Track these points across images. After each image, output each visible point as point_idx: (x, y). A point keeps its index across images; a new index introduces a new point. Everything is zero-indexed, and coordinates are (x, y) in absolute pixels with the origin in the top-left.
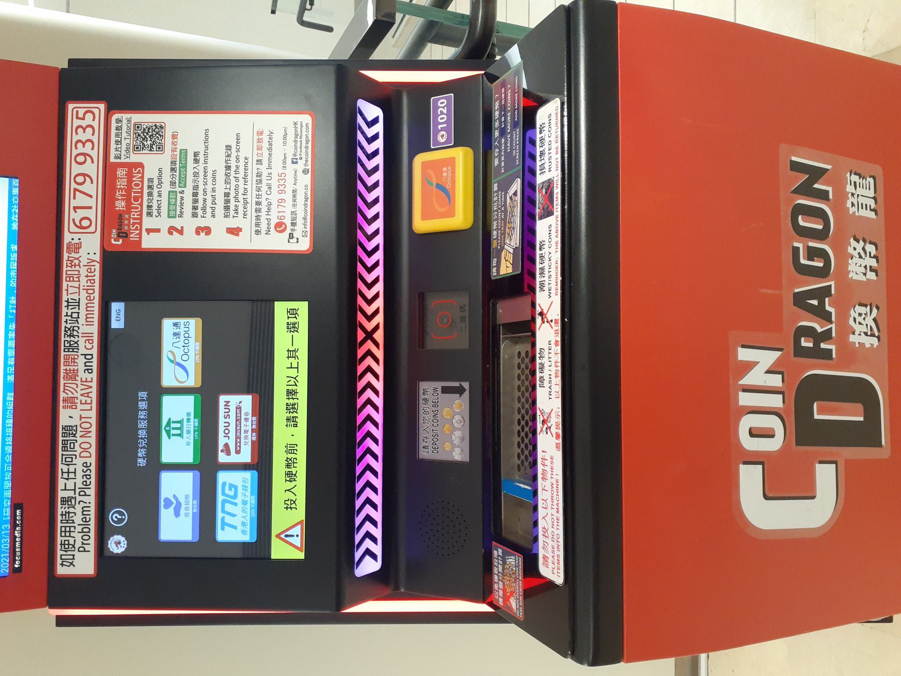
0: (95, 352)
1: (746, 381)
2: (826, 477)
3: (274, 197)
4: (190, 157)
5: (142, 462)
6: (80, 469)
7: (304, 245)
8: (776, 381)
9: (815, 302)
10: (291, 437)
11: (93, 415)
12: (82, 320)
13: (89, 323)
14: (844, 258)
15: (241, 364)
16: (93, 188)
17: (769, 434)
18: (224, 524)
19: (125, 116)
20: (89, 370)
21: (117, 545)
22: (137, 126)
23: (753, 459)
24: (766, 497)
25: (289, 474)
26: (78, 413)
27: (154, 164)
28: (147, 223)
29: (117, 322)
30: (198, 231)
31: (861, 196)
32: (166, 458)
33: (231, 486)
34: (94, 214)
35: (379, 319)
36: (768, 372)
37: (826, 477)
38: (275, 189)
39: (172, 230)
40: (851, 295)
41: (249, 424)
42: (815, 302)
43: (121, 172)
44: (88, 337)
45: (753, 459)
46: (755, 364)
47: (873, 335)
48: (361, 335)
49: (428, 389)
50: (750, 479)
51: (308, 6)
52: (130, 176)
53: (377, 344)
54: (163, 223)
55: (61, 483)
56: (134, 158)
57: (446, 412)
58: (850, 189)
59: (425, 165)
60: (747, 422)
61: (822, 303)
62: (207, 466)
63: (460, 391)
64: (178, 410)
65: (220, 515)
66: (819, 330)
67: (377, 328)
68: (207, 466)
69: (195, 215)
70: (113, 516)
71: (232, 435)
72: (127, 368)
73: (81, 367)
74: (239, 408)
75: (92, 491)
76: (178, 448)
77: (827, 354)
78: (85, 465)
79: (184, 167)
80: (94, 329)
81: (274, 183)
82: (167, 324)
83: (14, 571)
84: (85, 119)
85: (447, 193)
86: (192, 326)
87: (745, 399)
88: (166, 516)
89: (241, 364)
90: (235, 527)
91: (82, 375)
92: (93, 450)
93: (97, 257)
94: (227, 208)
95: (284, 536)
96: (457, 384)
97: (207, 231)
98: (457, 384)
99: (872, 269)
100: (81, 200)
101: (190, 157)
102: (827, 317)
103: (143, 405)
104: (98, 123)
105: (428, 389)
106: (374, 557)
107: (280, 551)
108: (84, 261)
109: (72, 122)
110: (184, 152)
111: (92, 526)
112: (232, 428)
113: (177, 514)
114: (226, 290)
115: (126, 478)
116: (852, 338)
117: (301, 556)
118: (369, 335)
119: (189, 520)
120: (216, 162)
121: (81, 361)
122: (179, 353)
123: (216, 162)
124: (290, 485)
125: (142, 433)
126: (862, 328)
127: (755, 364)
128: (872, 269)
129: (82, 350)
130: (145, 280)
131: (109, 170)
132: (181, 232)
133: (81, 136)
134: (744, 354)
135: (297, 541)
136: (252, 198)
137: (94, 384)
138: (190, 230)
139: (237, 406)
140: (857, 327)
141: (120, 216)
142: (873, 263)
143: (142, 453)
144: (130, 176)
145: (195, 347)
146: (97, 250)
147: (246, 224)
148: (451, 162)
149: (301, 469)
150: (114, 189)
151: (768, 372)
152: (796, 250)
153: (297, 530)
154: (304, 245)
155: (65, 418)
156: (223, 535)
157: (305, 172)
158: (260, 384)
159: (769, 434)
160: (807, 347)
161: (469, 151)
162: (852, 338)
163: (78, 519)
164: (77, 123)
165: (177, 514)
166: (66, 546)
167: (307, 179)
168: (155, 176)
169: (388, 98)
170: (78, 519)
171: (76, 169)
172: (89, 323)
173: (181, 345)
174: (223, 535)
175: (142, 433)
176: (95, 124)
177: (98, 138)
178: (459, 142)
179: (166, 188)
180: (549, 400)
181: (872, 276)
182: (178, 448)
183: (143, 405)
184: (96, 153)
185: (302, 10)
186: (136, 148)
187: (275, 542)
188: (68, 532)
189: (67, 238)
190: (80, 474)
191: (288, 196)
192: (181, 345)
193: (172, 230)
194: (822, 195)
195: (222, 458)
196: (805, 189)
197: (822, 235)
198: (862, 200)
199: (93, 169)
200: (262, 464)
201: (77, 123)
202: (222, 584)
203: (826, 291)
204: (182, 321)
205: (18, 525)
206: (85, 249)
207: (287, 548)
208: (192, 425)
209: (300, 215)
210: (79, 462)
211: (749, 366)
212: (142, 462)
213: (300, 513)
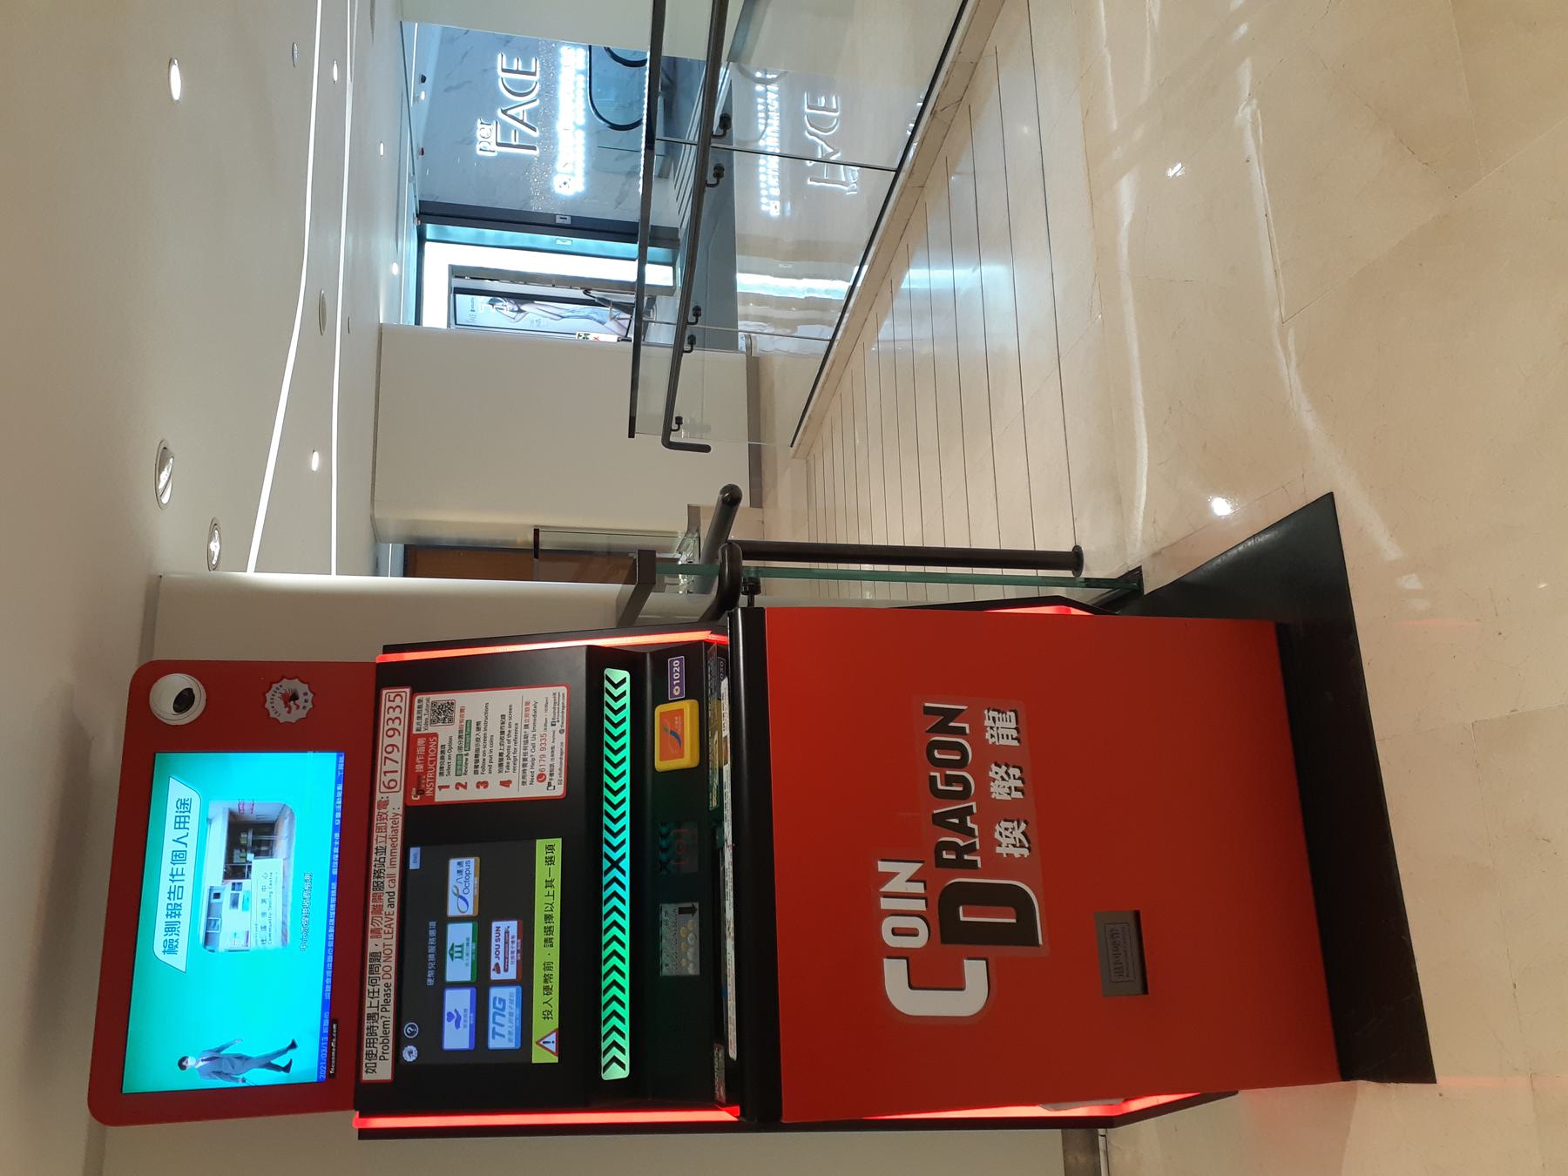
0: (396, 890)
1: (888, 887)
2: (975, 972)
3: (537, 754)
4: (474, 726)
5: (430, 982)
6: (382, 988)
7: (559, 791)
8: (918, 888)
9: (956, 821)
10: (548, 955)
11: (393, 943)
12: (387, 864)
13: (393, 866)
14: (985, 782)
15: (506, 895)
16: (399, 756)
17: (913, 933)
18: (495, 1033)
19: (424, 697)
20: (391, 905)
21: (410, 1054)
22: (434, 704)
23: (897, 954)
25: (546, 988)
26: (382, 942)
27: (446, 733)
28: (440, 781)
29: (414, 865)
30: (479, 785)
31: (1002, 728)
33: (502, 1001)
34: (399, 777)
35: (626, 849)
36: (909, 881)
37: (975, 972)
38: (538, 747)
39: (458, 785)
42: (956, 821)
43: (421, 742)
44: (391, 876)
45: (897, 954)
46: (894, 875)
47: (1022, 846)
48: (606, 864)
50: (895, 974)
51: (674, 426)
52: (427, 744)
53: (623, 872)
54: (451, 780)
55: (368, 1002)
56: (431, 730)
58: (988, 723)
60: (888, 924)
61: (963, 821)
62: (481, 984)
63: (691, 911)
64: (460, 935)
65: (491, 1025)
66: (962, 844)
67: (623, 856)
68: (481, 984)
69: (476, 772)
70: (407, 1029)
71: (502, 956)
72: (422, 902)
73: (386, 903)
74: (507, 933)
75: (391, 1008)
76: (459, 969)
78: (387, 985)
79: (469, 734)
80: (396, 871)
81: (537, 742)
83: (328, 1074)
84: (395, 701)
85: (679, 738)
86: (471, 864)
87: (886, 904)
88: (449, 1027)
89: (506, 895)
90: (503, 1037)
91: (386, 909)
92: (393, 973)
93: (400, 812)
94: (501, 765)
95: (542, 1043)
96: (689, 905)
97: (485, 784)
98: (689, 905)
99: (1017, 789)
100: (389, 766)
101: (474, 726)
102: (971, 832)
103: (432, 933)
104: (405, 704)
105: (668, 912)
106: (622, 1065)
108: (390, 815)
109: (385, 704)
110: (469, 722)
111: (391, 1036)
112: (502, 950)
113: (457, 1025)
114: (498, 830)
115: (419, 999)
116: (998, 850)
117: (555, 1059)
118: (615, 864)
119: (467, 1030)
120: (494, 729)
121: (386, 897)
123: (494, 729)
124: (547, 998)
125: (431, 957)
126: (1010, 840)
127: (894, 875)
128: (1017, 789)
129: (387, 889)
130: (439, 828)
131: (412, 740)
132: (465, 787)
133: (392, 715)
134: (883, 867)
135: (553, 1047)
136: (520, 757)
137: (395, 917)
138: (472, 785)
140: (1004, 841)
141: (419, 776)
142: (1019, 784)
143: (430, 974)
144: (427, 744)
145: (473, 881)
146: (400, 804)
147: (514, 777)
148: (681, 712)
149: (555, 983)
150: (415, 755)
151: (909, 881)
153: (553, 1037)
154: (559, 791)
155: (373, 945)
156: (494, 1043)
157: (561, 732)
159: (913, 933)
160: (936, 862)
161: (695, 702)
162: (998, 850)
163: (380, 1032)
164: (389, 704)
165: (457, 1025)
166: (370, 1055)
167: (562, 738)
168: (446, 743)
170: (380, 1032)
171: (387, 741)
172: (393, 866)
173: (463, 879)
174: (494, 1043)
175: (431, 957)
176: (400, 728)
177: (404, 716)
178: (688, 696)
179: (455, 751)
180: (729, 914)
181: (1019, 795)
182: (459, 969)
183: (432, 933)
184: (402, 728)
185: (667, 431)
186: (433, 722)
187: (535, 1048)
188: (372, 1043)
189: (378, 797)
190: (382, 993)
191: (548, 752)
192: (463, 879)
193: (458, 785)
194: (960, 732)
195: (494, 976)
196: (942, 728)
197: (960, 764)
198: (1005, 732)
199: (400, 740)
200: (524, 980)
201: (389, 704)
202: (492, 1082)
203: (969, 810)
204: (464, 860)
205: (586, 292)
206: (391, 803)
207: (544, 1054)
208: (470, 948)
209: (557, 767)
210: (382, 983)
211: (890, 876)
212: (430, 982)
213: (554, 1023)
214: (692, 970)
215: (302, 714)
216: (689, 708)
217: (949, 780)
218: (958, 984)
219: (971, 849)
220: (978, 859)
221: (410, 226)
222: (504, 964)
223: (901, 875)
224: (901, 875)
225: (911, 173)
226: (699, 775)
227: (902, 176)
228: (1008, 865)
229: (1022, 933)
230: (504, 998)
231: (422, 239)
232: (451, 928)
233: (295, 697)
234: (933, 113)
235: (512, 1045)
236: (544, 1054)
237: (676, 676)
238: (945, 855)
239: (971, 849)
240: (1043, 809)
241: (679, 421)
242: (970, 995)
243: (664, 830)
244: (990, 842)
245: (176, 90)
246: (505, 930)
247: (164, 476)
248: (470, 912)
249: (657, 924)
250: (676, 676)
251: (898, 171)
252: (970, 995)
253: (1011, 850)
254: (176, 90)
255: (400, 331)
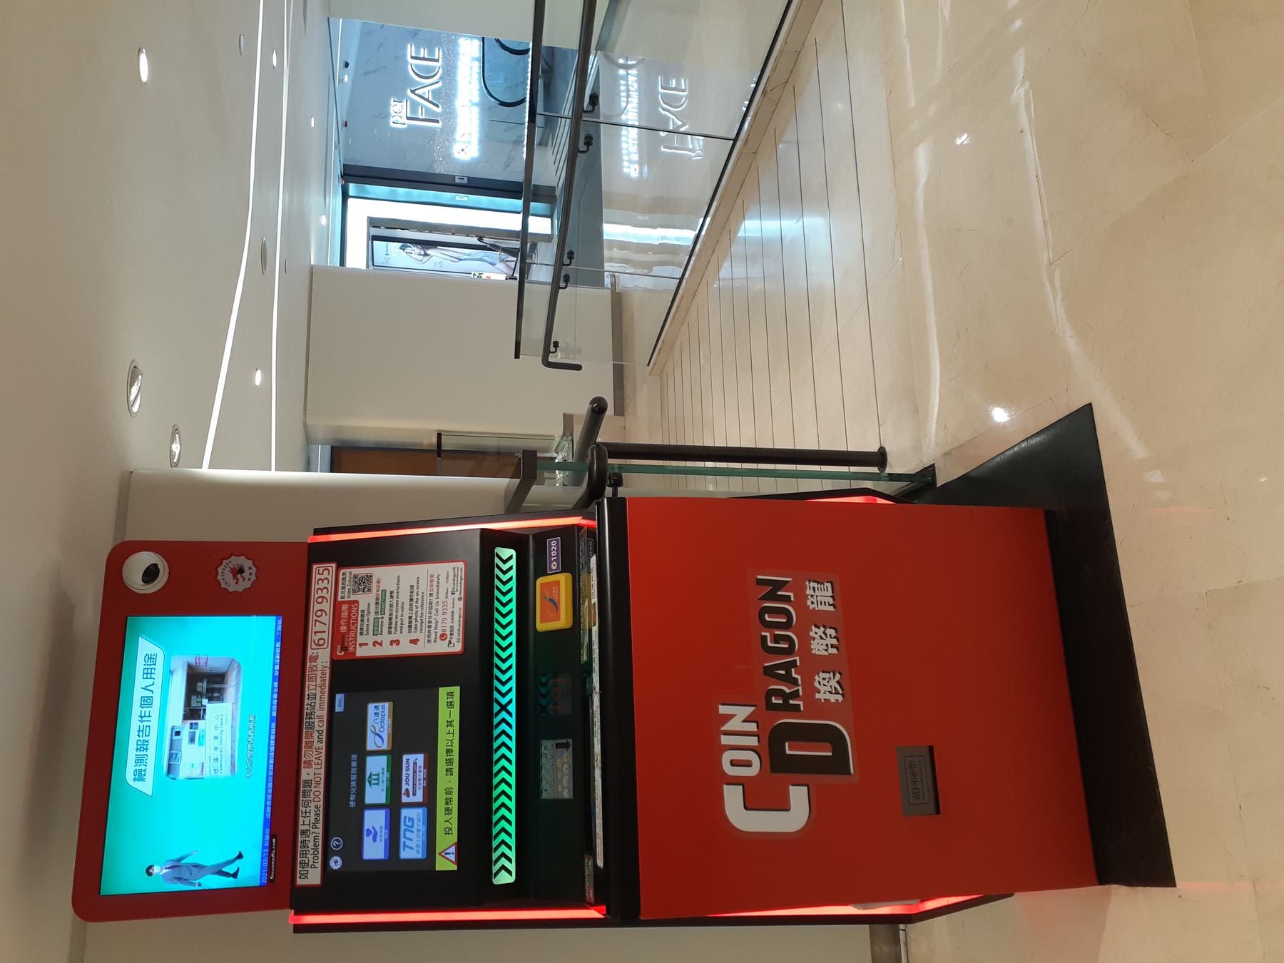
0: (324, 728)
1: (727, 727)
2: (799, 796)
3: (440, 618)
4: (388, 594)
5: (352, 804)
6: (313, 809)
7: (458, 648)
8: (752, 727)
9: (783, 672)
10: (448, 782)
11: (322, 772)
12: (317, 707)
13: (322, 709)
14: (806, 640)
15: (414, 733)
16: (327, 619)
17: (748, 764)
18: (405, 846)
19: (347, 571)
20: (320, 741)
21: (336, 863)
22: (355, 576)
23: (734, 781)
25: (447, 809)
26: (313, 772)
27: (365, 601)
28: (360, 640)
29: (339, 708)
30: (392, 643)
31: (820, 596)
33: (411, 819)
34: (327, 636)
35: (513, 695)
36: (744, 721)
37: (799, 796)
38: (440, 612)
39: (375, 643)
42: (783, 672)
43: (345, 607)
44: (320, 718)
45: (734, 781)
46: (732, 716)
47: (837, 693)
48: (496, 708)
50: (733, 797)
51: (552, 349)
52: (350, 609)
53: (510, 714)
54: (370, 639)
55: (301, 820)
56: (353, 598)
58: (809, 592)
60: (727, 757)
61: (789, 672)
62: (394, 806)
63: (566, 746)
64: (377, 766)
65: (402, 839)
66: (788, 691)
67: (510, 701)
68: (394, 806)
69: (390, 633)
70: (333, 843)
71: (411, 783)
72: (346, 739)
73: (316, 740)
74: (415, 764)
75: (320, 825)
76: (376, 793)
78: (317, 807)
79: (384, 601)
80: (325, 713)
81: (440, 608)
83: (269, 880)
84: (323, 574)
85: (556, 605)
86: (386, 707)
87: (725, 740)
88: (367, 841)
89: (414, 733)
90: (412, 849)
91: (316, 744)
92: (321, 797)
93: (328, 665)
94: (410, 626)
95: (444, 854)
96: (564, 741)
97: (397, 642)
98: (564, 741)
99: (832, 646)
100: (319, 627)
101: (388, 594)
102: (795, 682)
103: (354, 764)
104: (332, 577)
105: (547, 747)
106: (509, 872)
108: (320, 667)
109: (315, 576)
110: (384, 592)
111: (320, 848)
112: (411, 778)
113: (375, 840)
114: (408, 680)
115: (343, 818)
116: (817, 696)
117: (455, 868)
118: (504, 708)
119: (383, 844)
120: (404, 597)
121: (316, 735)
123: (404, 597)
124: (448, 817)
125: (353, 784)
126: (827, 687)
127: (732, 716)
128: (832, 646)
129: (317, 728)
130: (359, 678)
131: (337, 606)
132: (381, 644)
133: (321, 585)
134: (723, 710)
135: (453, 857)
136: (426, 620)
137: (323, 751)
138: (386, 643)
140: (822, 689)
141: (343, 636)
142: (835, 642)
143: (352, 797)
144: (350, 609)
145: (388, 721)
146: (328, 659)
147: (421, 636)
148: (557, 583)
149: (455, 805)
150: (340, 618)
151: (744, 721)
153: (453, 849)
154: (458, 648)
155: (305, 774)
156: (405, 854)
157: (460, 599)
159: (748, 764)
160: (766, 706)
161: (569, 575)
162: (817, 696)
163: (311, 845)
164: (318, 577)
165: (375, 840)
166: (303, 864)
167: (460, 604)
168: (365, 608)
170: (311, 845)
171: (317, 607)
172: (322, 709)
173: (379, 720)
174: (405, 854)
175: (353, 784)
176: (328, 596)
177: (331, 586)
178: (564, 570)
179: (373, 615)
180: (597, 748)
181: (834, 651)
182: (376, 793)
183: (354, 764)
184: (329, 596)
185: (546, 353)
186: (354, 591)
187: (438, 859)
188: (304, 854)
189: (310, 652)
190: (313, 813)
191: (449, 616)
192: (379, 720)
193: (375, 643)
194: (786, 599)
195: (405, 799)
196: (771, 596)
197: (786, 626)
198: (823, 599)
199: (327, 606)
200: (429, 802)
201: (318, 577)
202: (403, 886)
203: (793, 663)
204: (380, 704)
205: (480, 239)
206: (321, 658)
207: (446, 863)
208: (385, 777)
209: (456, 628)
210: (312, 805)
211: (729, 717)
212: (352, 804)
213: (454, 838)
214: (567, 794)
215: (248, 584)
216: (564, 580)
217: (777, 639)
218: (784, 806)
219: (795, 695)
220: (801, 703)
221: (336, 185)
222: (413, 790)
223: (738, 717)
224: (738, 717)
225: (746, 142)
226: (572, 635)
227: (739, 144)
228: (825, 708)
229: (837, 764)
230: (413, 818)
231: (345, 196)
232: (369, 760)
233: (241, 571)
234: (764, 92)
235: (419, 856)
236: (446, 863)
237: (554, 554)
238: (774, 700)
239: (795, 695)
240: (854, 662)
241: (556, 345)
242: (794, 815)
243: (544, 680)
244: (811, 690)
245: (144, 73)
246: (414, 761)
247: (134, 390)
248: (385, 747)
249: (538, 757)
250: (554, 554)
251: (735, 140)
252: (794, 815)
253: (828, 696)
254: (144, 73)
255: (327, 271)
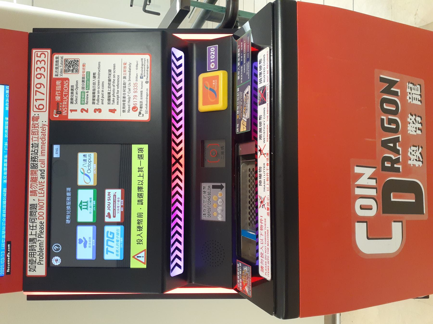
0: (46, 169)
1: (359, 182)
2: (397, 228)
3: (132, 95)
4: (92, 75)
5: (68, 222)
6: (38, 225)
7: (146, 117)
8: (373, 182)
9: (392, 145)
10: (140, 209)
11: (44, 199)
12: (39, 153)
13: (43, 155)
14: (406, 123)
15: (116, 175)
16: (45, 90)
17: (369, 208)
18: (108, 251)
19: (60, 56)
20: (43, 177)
21: (56, 261)
22: (66, 60)
23: (362, 220)
24: (368, 238)
25: (139, 227)
26: (38, 198)
27: (74, 79)
28: (71, 107)
29: (56, 155)
30: (95, 110)
31: (414, 94)
32: (80, 220)
33: (111, 233)
34: (45, 103)
35: (182, 153)
36: (369, 178)
37: (397, 228)
38: (132, 91)
39: (82, 110)
40: (409, 142)
41: (120, 203)
42: (392, 145)
43: (58, 83)
44: (42, 162)
45: (362, 220)
46: (363, 174)
47: (419, 161)
48: (173, 161)
49: (206, 187)
50: (360, 229)
51: (148, 3)
52: (62, 84)
53: (181, 165)
54: (78, 107)
55: (29, 232)
56: (65, 76)
57: (214, 198)
58: (408, 90)
59: (204, 79)
60: (359, 202)
61: (395, 145)
62: (99, 223)
63: (221, 187)
64: (86, 196)
65: (106, 247)
66: (394, 158)
67: (181, 157)
68: (99, 223)
69: (94, 103)
70: (54, 247)
71: (112, 208)
72: (61, 176)
73: (39, 176)
74: (115, 196)
75: (44, 235)
76: (85, 215)
77: (398, 170)
78: (41, 223)
79: (89, 80)
80: (45, 158)
81: (132, 88)
82: (80, 155)
83: (7, 274)
84: (41, 57)
85: (215, 92)
86: (92, 156)
87: (358, 191)
88: (80, 247)
89: (116, 175)
90: (113, 252)
91: (39, 180)
92: (45, 216)
93: (47, 123)
94: (109, 100)
95: (137, 257)
96: (219, 184)
97: (100, 110)
98: (219, 184)
99: (419, 129)
100: (39, 96)
101: (92, 75)
102: (397, 152)
103: (69, 194)
104: (47, 59)
105: (206, 187)
106: (180, 267)
107: (135, 264)
108: (40, 125)
109: (35, 59)
110: (88, 73)
111: (44, 252)
112: (112, 205)
113: (85, 246)
114: (109, 139)
115: (61, 229)
116: (410, 162)
117: (145, 266)
118: (177, 161)
119: (91, 249)
120: (104, 78)
121: (39, 173)
122: (86, 169)
123: (104, 78)
124: (139, 233)
125: (68, 208)
126: (414, 157)
127: (363, 174)
128: (419, 129)
129: (39, 168)
130: (70, 134)
131: (52, 82)
132: (87, 111)
133: (39, 65)
134: (358, 170)
135: (143, 259)
136: (121, 95)
137: (45, 184)
138: (91, 110)
139: (114, 195)
140: (412, 157)
141: (58, 103)
142: (420, 126)
143: (68, 217)
144: (62, 84)
145: (94, 166)
146: (47, 120)
147: (118, 108)
148: (217, 78)
149: (145, 225)
150: (55, 90)
151: (369, 178)
152: (382, 120)
153: (143, 254)
154: (146, 117)
155: (31, 200)
156: (107, 257)
157: (147, 82)
158: (125, 184)
159: (369, 208)
160: (388, 166)
161: (225, 72)
162: (410, 162)
163: (37, 249)
164: (37, 59)
165: (85, 246)
166: (32, 262)
167: (147, 86)
168: (74, 84)
169: (186, 47)
170: (37, 249)
171: (37, 81)
172: (43, 155)
173: (87, 165)
174: (107, 257)
175: (68, 208)
176: (46, 60)
177: (47, 66)
178: (221, 68)
179: (80, 90)
180: (264, 192)
181: (419, 132)
182: (85, 215)
183: (69, 194)
184: (46, 73)
185: (145, 5)
186: (66, 71)
187: (132, 260)
188: (33, 255)
189: (32, 114)
190: (38, 227)
191: (139, 94)
192: (87, 165)
193: (82, 110)
194: (395, 94)
195: (107, 220)
196: (387, 91)
197: (395, 113)
198: (414, 96)
199: (45, 81)
200: (126, 222)
201: (37, 59)
202: (106, 280)
203: (397, 140)
204: (87, 154)
205: (9, 252)
206: (41, 119)
207: (138, 263)
208: (92, 204)
209: (144, 103)
210: (38, 221)
211: (360, 175)
212: (68, 222)
213: (144, 246)
